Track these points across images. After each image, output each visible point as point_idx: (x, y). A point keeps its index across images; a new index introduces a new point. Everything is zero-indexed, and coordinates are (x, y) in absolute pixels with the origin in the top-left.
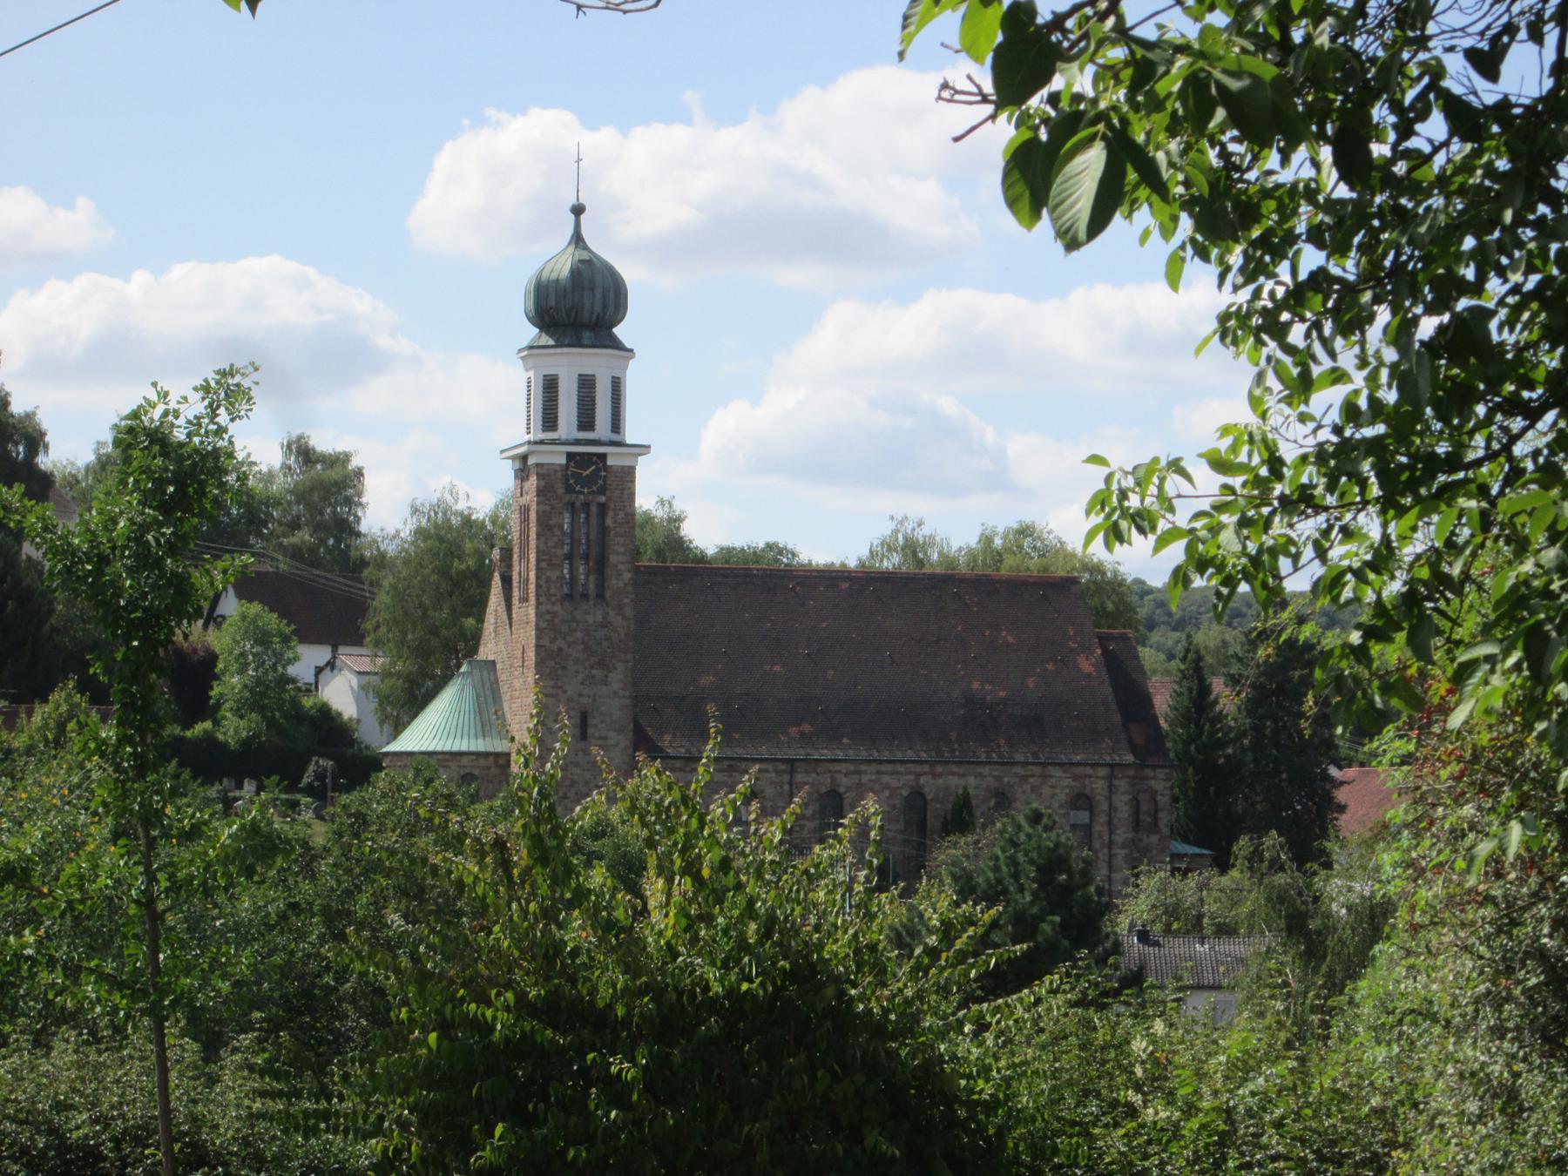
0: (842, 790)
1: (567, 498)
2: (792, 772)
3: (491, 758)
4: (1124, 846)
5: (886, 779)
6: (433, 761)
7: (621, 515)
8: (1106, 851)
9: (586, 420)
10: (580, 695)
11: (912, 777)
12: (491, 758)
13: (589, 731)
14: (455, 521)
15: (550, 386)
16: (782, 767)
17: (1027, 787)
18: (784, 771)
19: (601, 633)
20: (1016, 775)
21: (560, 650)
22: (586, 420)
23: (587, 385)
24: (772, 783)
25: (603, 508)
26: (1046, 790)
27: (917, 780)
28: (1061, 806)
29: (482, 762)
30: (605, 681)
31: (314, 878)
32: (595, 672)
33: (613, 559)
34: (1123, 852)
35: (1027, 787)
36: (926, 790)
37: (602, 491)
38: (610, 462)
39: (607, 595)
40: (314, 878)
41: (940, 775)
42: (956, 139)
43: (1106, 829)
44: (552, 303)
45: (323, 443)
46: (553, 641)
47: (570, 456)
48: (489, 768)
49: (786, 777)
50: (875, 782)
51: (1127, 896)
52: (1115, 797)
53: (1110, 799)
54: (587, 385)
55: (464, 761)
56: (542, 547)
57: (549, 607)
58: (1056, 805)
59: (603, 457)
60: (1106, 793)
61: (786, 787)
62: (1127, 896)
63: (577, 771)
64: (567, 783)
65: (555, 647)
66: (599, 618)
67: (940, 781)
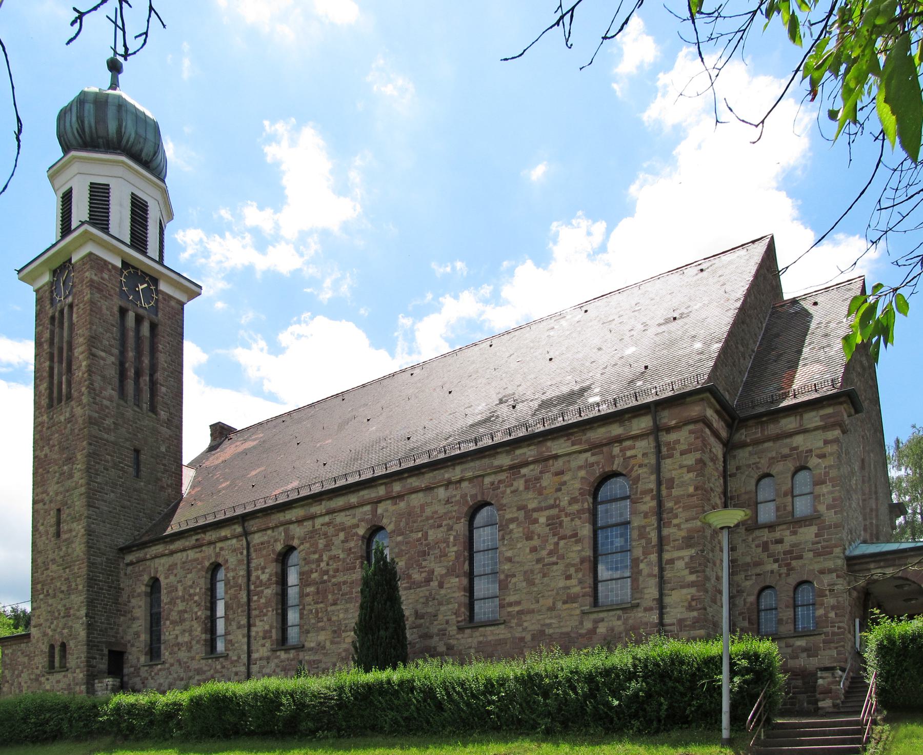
4: (688, 542)
5: (340, 518)
6: (40, 560)
9: (139, 240)
14: (810, 154)
15: (99, 195)
17: (520, 484)
20: (500, 470)
24: (235, 550)
26: (547, 480)
27: (374, 511)
28: (573, 501)
31: (570, 504)
34: (687, 553)
35: (520, 484)
38: (163, 287)
40: (570, 504)
42: (164, 26)
45: (684, 151)
50: (328, 524)
51: (663, 660)
52: (667, 464)
53: (658, 470)
54: (139, 209)
58: (564, 502)
59: (155, 281)
62: (663, 660)
67: (402, 505)
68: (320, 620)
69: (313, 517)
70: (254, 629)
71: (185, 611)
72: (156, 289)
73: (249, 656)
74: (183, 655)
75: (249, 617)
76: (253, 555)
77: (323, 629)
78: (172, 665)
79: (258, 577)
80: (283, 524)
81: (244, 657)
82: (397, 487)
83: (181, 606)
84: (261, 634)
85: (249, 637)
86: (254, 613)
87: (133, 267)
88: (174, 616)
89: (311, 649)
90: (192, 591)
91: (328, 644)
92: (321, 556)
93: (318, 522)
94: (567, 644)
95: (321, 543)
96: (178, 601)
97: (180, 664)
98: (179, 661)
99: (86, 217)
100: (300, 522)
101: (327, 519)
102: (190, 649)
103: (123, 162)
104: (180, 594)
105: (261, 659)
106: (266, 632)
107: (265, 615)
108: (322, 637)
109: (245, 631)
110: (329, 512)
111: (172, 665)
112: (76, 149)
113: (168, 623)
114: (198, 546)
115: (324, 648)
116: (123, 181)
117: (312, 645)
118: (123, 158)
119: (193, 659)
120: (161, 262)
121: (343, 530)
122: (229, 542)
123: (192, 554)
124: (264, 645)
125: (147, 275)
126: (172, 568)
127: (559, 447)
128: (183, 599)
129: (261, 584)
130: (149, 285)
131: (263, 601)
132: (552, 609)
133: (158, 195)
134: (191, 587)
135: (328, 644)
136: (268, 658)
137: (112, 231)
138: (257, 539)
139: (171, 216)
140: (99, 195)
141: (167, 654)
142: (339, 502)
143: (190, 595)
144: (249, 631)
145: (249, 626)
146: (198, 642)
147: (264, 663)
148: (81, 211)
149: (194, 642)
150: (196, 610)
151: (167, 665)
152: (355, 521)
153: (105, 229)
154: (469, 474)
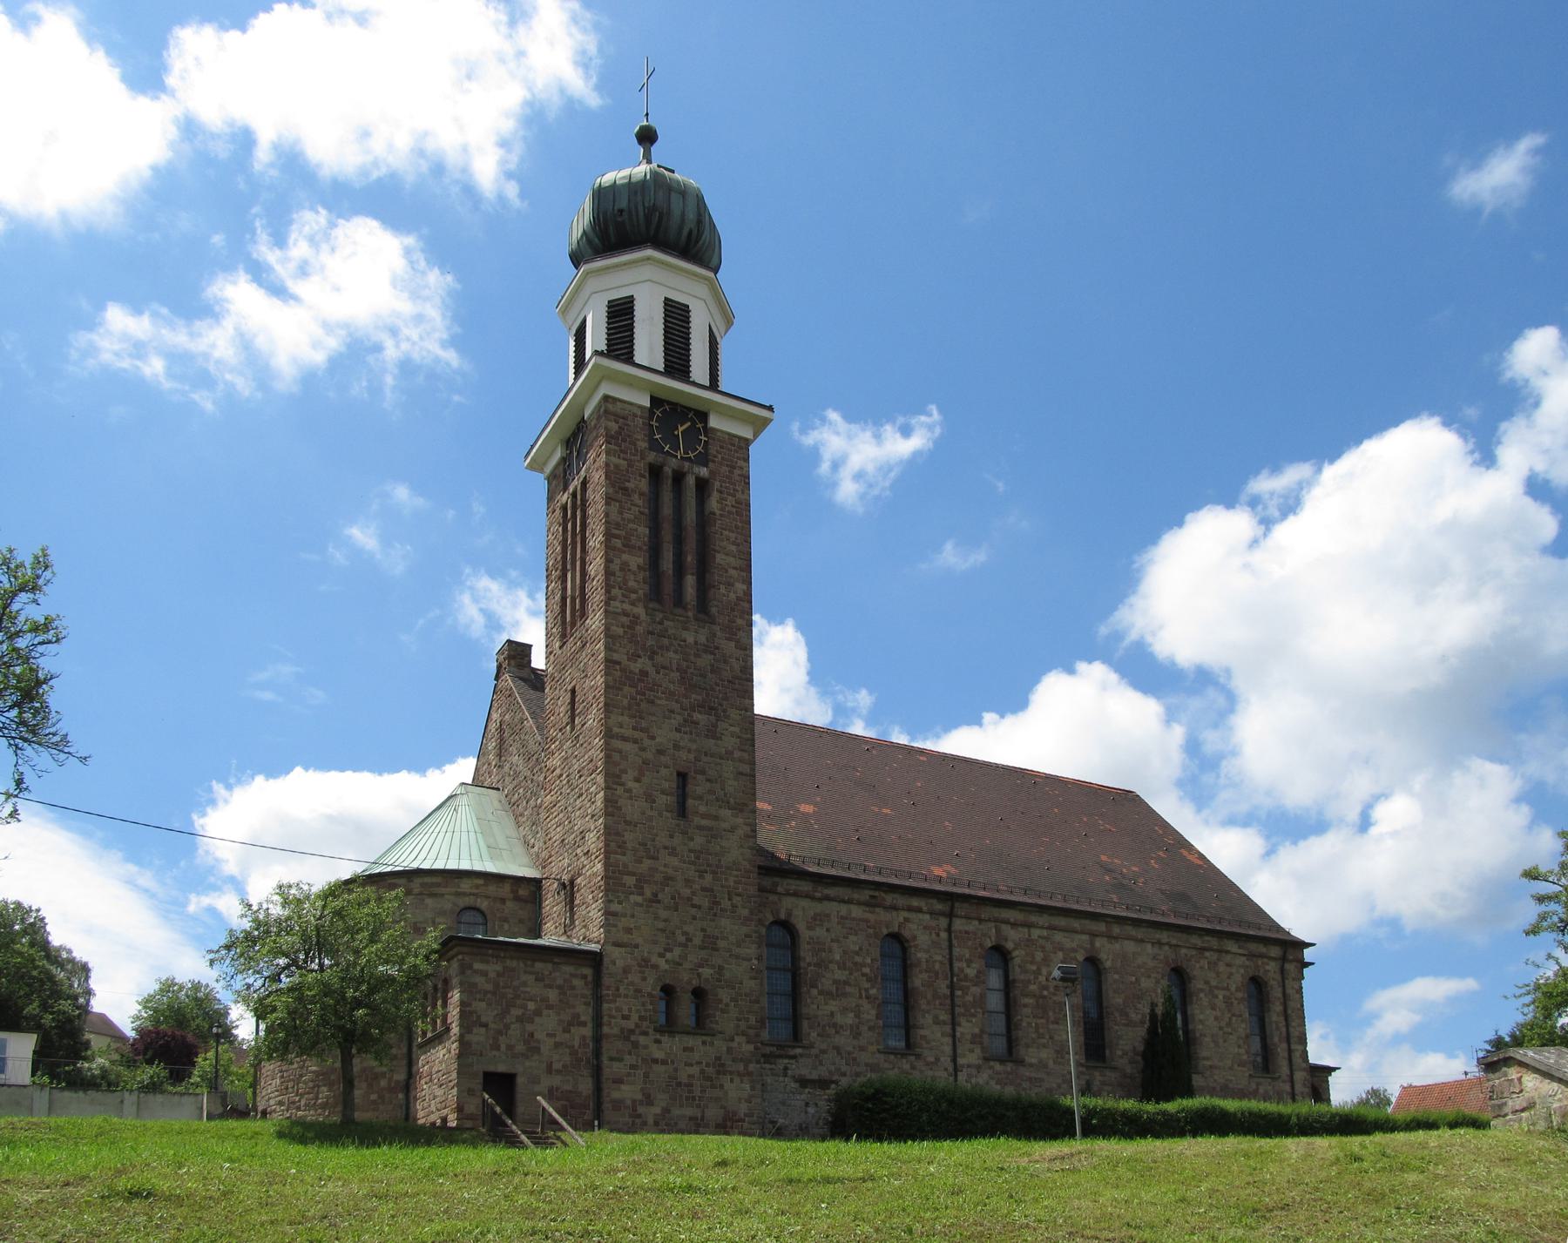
0: (1010, 945)
1: (652, 457)
2: (951, 915)
3: (507, 887)
7: (730, 501)
8: (1284, 1045)
9: (677, 364)
10: (676, 747)
11: (1085, 937)
12: (507, 887)
13: (690, 802)
15: (621, 314)
16: (939, 906)
17: (1204, 963)
18: (942, 914)
19: (705, 660)
21: (644, 673)
22: (677, 364)
23: (676, 318)
25: (702, 486)
26: (1222, 968)
28: (1238, 989)
29: (492, 889)
30: (713, 733)
32: (696, 716)
33: (720, 558)
35: (1204, 963)
36: (1103, 956)
37: (703, 460)
38: (714, 422)
39: (714, 610)
41: (1116, 938)
43: (1282, 1019)
44: (623, 204)
46: (634, 657)
47: (656, 401)
48: (503, 901)
49: (944, 922)
50: (1047, 938)
54: (676, 318)
55: (466, 885)
56: (614, 516)
57: (627, 607)
58: (1233, 988)
59: (704, 416)
60: (1278, 977)
61: (944, 935)
63: (674, 861)
64: (658, 877)
65: (636, 666)
66: (702, 639)
67: (1117, 946)
68: (1041, 1036)
69: (1030, 926)
70: (959, 1029)
71: (846, 983)
72: (705, 427)
73: (954, 1060)
74: (843, 1040)
75: (953, 1014)
76: (955, 942)
77: (1044, 1046)
78: (823, 1052)
79: (962, 970)
80: (996, 920)
81: (946, 1061)
82: (1116, 930)
83: (840, 975)
84: (969, 1037)
85: (954, 1036)
86: (957, 1010)
87: (669, 403)
88: (826, 983)
89: (1031, 1065)
90: (858, 959)
91: (1051, 1063)
92: (1039, 969)
93: (1036, 933)
94: (1242, 1094)
95: (1039, 956)
96: (833, 966)
97: (839, 1053)
98: (837, 1049)
99: (603, 347)
100: (1014, 925)
101: (1045, 933)
102: (857, 1035)
103: (648, 259)
104: (837, 957)
105: (969, 1066)
106: (974, 1036)
107: (973, 1015)
108: (1044, 1054)
109: (948, 1029)
110: (1051, 928)
111: (823, 1052)
112: (587, 262)
113: (814, 992)
114: (872, 904)
115: (1046, 1066)
116: (649, 281)
117: (1034, 1061)
118: (649, 252)
119: (862, 1049)
120: (714, 385)
121: (1061, 949)
122: (921, 916)
123: (857, 912)
124: (972, 1051)
125: (690, 409)
126: (818, 919)
127: (1232, 946)
128: (842, 966)
129: (966, 978)
130: (694, 423)
131: (969, 998)
132: (1231, 1068)
133: (702, 290)
134: (857, 953)
135: (1051, 1063)
136: (978, 1068)
137: (637, 359)
138: (958, 924)
139: (729, 321)
140: (621, 314)
141: (814, 1034)
142: (1061, 921)
143: (856, 964)
144: (954, 1030)
145: (954, 1024)
146: (870, 1029)
147: (974, 1071)
148: (595, 339)
149: (864, 1028)
150: (867, 985)
151: (814, 1051)
152: (1074, 945)
153: (628, 358)
154: (1174, 942)
